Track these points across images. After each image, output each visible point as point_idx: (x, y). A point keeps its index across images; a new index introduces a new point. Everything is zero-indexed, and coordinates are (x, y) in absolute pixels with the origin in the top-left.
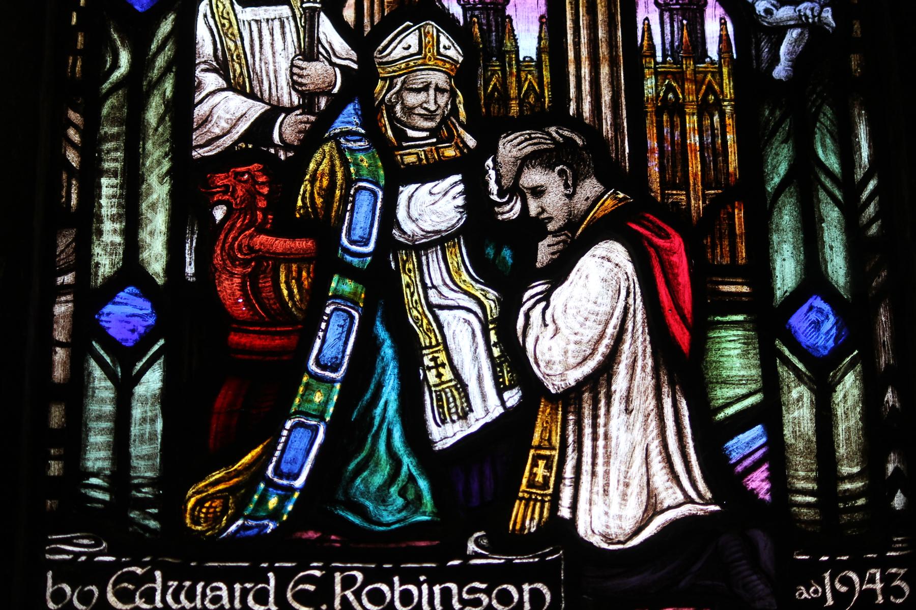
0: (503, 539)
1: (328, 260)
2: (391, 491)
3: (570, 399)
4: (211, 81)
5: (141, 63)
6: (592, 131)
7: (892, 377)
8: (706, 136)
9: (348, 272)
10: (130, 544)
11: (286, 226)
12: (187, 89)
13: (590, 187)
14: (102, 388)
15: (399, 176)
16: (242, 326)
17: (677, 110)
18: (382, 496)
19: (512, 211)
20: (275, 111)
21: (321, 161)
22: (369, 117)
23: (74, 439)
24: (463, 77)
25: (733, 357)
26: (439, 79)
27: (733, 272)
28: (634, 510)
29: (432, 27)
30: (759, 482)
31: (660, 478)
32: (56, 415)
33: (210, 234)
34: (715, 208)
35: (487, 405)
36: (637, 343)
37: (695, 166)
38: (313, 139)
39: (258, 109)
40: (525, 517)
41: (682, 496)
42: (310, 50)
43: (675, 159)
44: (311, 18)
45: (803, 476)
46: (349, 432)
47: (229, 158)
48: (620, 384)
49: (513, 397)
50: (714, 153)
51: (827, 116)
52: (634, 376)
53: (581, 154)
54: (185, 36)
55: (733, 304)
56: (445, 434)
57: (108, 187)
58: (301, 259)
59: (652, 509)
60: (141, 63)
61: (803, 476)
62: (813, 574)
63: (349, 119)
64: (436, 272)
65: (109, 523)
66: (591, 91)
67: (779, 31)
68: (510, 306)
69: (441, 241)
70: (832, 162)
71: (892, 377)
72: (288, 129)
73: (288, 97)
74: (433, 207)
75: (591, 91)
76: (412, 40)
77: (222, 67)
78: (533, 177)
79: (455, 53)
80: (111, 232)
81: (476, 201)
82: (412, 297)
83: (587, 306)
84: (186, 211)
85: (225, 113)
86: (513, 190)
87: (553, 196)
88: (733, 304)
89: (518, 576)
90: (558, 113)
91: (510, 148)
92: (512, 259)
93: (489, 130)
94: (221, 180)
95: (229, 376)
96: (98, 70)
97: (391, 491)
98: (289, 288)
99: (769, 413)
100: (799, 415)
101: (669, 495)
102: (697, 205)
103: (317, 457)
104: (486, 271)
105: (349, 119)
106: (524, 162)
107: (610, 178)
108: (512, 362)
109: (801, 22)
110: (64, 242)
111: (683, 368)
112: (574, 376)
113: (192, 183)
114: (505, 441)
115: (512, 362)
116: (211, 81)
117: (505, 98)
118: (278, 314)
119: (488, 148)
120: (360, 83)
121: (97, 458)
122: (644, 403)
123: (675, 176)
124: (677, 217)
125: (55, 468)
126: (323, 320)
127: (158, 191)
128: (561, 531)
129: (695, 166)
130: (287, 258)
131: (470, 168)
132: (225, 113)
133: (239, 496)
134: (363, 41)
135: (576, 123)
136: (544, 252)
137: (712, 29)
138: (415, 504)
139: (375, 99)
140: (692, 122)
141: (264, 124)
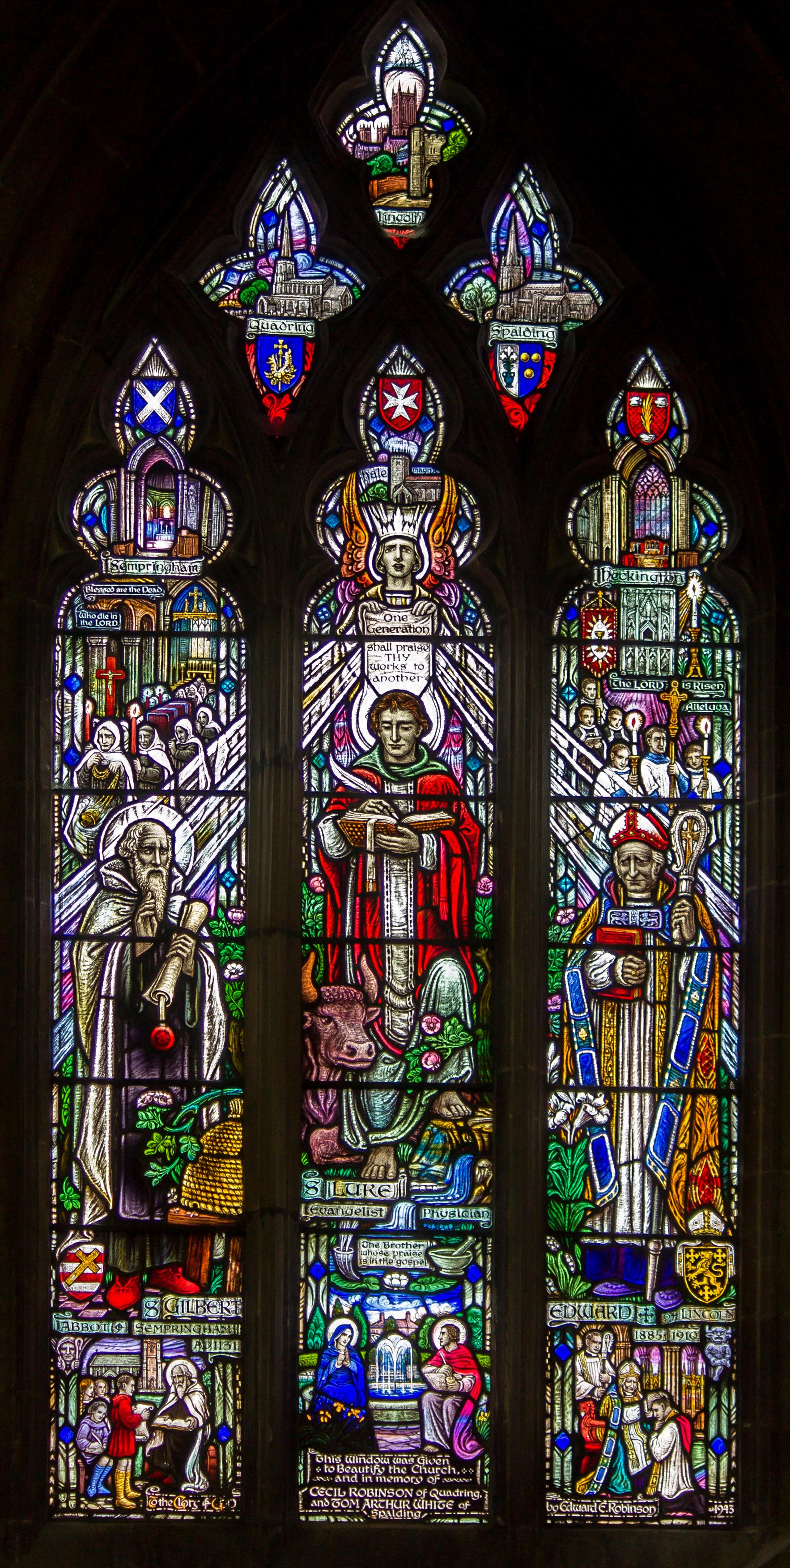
0: (646, 1496)
1: (607, 1427)
2: (621, 1484)
3: (661, 1462)
4: (580, 1378)
5: (563, 1374)
6: (669, 1394)
7: (735, 1459)
8: (696, 1395)
9: (612, 1429)
10: (565, 1496)
11: (598, 1418)
12: (575, 1380)
13: (669, 1409)
14: (557, 1458)
15: (624, 1405)
16: (589, 1443)
17: (689, 1388)
18: (619, 1485)
19: (650, 1415)
20: (596, 1387)
21: (606, 1401)
22: (617, 1389)
23: (551, 1471)
24: (640, 1379)
25: (699, 1451)
26: (634, 1379)
27: (700, 1431)
28: (674, 1489)
29: (633, 1364)
30: (702, 1484)
31: (681, 1482)
32: (548, 1465)
33: (581, 1419)
34: (698, 1414)
35: (644, 1464)
36: (678, 1449)
37: (693, 1403)
38: (604, 1395)
39: (592, 1387)
40: (650, 1491)
41: (686, 1487)
42: (603, 1371)
43: (689, 1401)
44: (604, 1361)
45: (712, 1482)
46: (612, 1470)
47: (585, 1400)
48: (673, 1459)
49: (649, 1462)
50: (698, 1400)
51: (725, 1391)
52: (677, 1456)
53: (668, 1400)
54: (573, 1366)
55: (699, 1440)
56: (634, 1471)
57: (557, 1407)
58: (601, 1427)
59: (679, 1489)
60: (563, 1374)
61: (712, 1482)
62: (712, 1505)
63: (613, 1391)
64: (632, 1431)
65: (560, 1491)
66: (670, 1383)
67: (715, 1367)
68: (649, 1439)
69: (634, 1422)
70: (726, 1404)
71: (735, 1459)
72: (598, 1392)
73: (599, 1384)
74: (632, 1413)
75: (670, 1383)
76: (628, 1368)
77: (583, 1375)
78: (655, 1406)
79: (638, 1372)
80: (558, 1419)
81: (642, 1412)
82: (627, 1436)
83: (667, 1438)
84: (576, 1413)
85: (584, 1387)
86: (651, 1409)
87: (660, 1410)
88: (699, 1440)
89: (648, 1504)
90: (662, 1389)
91: (651, 1397)
92: (648, 1425)
93: (645, 1392)
94: (583, 1405)
95: (586, 1458)
96: (553, 1376)
97: (621, 1484)
98: (599, 1434)
99: (706, 1467)
100: (713, 1468)
101: (682, 1486)
102: (693, 1414)
103: (114, 1027)
104: (644, 1430)
105: (613, 1391)
106: (654, 1402)
107: (673, 1405)
108: (649, 1452)
109: (721, 1364)
110: (548, 1421)
111: (687, 1455)
112: (663, 1457)
113: (576, 1406)
114: (647, 1473)
115: (649, 1452)
116: (580, 1378)
117: (649, 1384)
118: (596, 1441)
119: (645, 1397)
120: (615, 1380)
121: (557, 1476)
122: (678, 1463)
123: (688, 1407)
124: (688, 1416)
125: (548, 1478)
126: (54, 806)
127: (569, 1409)
128: (658, 1494)
129: (693, 1403)
130: (598, 1426)
131: (641, 1403)
132: (584, 1387)
133: (589, 1484)
134: (616, 1368)
135: (666, 1392)
136: (657, 1425)
137: (700, 1366)
138: (626, 1487)
139: (246, 766)
140: (693, 1391)
141: (593, 1390)
